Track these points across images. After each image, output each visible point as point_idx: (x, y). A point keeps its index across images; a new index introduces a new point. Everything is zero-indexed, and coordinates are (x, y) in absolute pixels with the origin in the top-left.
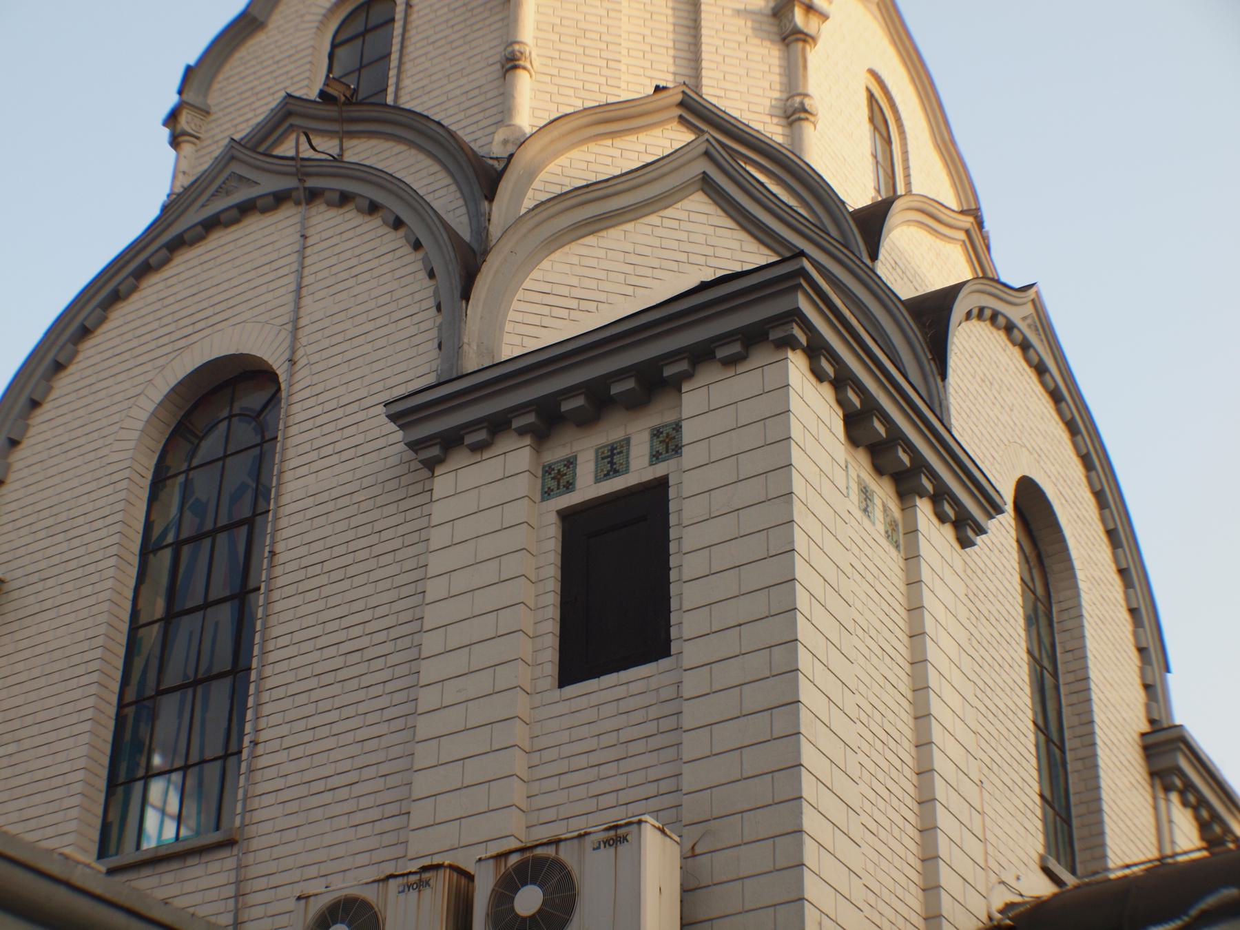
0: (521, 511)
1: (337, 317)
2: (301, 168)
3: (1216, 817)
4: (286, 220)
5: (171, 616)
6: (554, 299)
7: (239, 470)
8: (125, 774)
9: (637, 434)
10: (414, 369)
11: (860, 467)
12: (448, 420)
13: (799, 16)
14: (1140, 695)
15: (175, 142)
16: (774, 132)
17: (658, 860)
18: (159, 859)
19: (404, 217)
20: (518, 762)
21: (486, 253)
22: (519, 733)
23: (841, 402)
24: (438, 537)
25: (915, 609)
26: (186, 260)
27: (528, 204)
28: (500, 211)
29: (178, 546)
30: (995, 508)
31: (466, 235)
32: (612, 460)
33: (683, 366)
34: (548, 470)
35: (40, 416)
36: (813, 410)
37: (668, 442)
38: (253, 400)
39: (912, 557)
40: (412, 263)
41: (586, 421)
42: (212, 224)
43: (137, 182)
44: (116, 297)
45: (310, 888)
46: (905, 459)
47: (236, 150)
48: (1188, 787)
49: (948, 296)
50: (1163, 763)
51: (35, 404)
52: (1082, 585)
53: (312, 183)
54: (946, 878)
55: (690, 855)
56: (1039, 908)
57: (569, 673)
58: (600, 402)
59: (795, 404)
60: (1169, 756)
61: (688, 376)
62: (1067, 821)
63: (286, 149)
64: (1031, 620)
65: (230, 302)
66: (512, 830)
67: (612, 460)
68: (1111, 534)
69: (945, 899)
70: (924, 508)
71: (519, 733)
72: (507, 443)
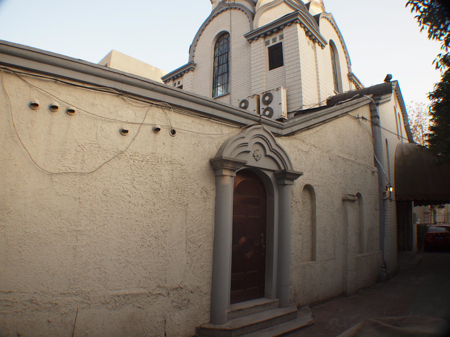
0: (263, 48)
1: (236, 24)
2: (229, 5)
3: (358, 85)
4: (228, 12)
5: (218, 66)
6: (265, 19)
7: (225, 46)
8: (215, 87)
9: (277, 36)
10: (247, 30)
11: (308, 39)
12: (252, 37)
14: (347, 69)
15: (212, 3)
17: (283, 92)
18: (220, 97)
19: (244, 10)
20: (265, 81)
21: (255, 14)
22: (264, 77)
23: (305, 30)
24: (252, 52)
26: (215, 19)
27: (260, 7)
28: (257, 8)
29: (218, 57)
30: (326, 44)
31: (252, 11)
32: (274, 40)
34: (266, 42)
35: (198, 42)
36: (301, 32)
37: (282, 37)
38: (226, 36)
39: (315, 51)
40: (245, 16)
41: (270, 35)
42: (218, 14)
43: (208, 9)
44: (207, 25)
45: (239, 99)
47: (220, 4)
48: (354, 81)
49: (319, 15)
50: (350, 78)
51: (198, 40)
52: (339, 54)
53: (231, 7)
54: (321, 93)
55: (287, 91)
56: (334, 97)
57: (270, 70)
58: (272, 32)
60: (351, 77)
61: (284, 28)
62: (337, 86)
63: (227, 2)
64: (332, 59)
65: (221, 24)
66: (265, 89)
67: (274, 40)
68: (343, 47)
69: (320, 88)
70: (317, 44)
71: (264, 77)
72: (260, 39)
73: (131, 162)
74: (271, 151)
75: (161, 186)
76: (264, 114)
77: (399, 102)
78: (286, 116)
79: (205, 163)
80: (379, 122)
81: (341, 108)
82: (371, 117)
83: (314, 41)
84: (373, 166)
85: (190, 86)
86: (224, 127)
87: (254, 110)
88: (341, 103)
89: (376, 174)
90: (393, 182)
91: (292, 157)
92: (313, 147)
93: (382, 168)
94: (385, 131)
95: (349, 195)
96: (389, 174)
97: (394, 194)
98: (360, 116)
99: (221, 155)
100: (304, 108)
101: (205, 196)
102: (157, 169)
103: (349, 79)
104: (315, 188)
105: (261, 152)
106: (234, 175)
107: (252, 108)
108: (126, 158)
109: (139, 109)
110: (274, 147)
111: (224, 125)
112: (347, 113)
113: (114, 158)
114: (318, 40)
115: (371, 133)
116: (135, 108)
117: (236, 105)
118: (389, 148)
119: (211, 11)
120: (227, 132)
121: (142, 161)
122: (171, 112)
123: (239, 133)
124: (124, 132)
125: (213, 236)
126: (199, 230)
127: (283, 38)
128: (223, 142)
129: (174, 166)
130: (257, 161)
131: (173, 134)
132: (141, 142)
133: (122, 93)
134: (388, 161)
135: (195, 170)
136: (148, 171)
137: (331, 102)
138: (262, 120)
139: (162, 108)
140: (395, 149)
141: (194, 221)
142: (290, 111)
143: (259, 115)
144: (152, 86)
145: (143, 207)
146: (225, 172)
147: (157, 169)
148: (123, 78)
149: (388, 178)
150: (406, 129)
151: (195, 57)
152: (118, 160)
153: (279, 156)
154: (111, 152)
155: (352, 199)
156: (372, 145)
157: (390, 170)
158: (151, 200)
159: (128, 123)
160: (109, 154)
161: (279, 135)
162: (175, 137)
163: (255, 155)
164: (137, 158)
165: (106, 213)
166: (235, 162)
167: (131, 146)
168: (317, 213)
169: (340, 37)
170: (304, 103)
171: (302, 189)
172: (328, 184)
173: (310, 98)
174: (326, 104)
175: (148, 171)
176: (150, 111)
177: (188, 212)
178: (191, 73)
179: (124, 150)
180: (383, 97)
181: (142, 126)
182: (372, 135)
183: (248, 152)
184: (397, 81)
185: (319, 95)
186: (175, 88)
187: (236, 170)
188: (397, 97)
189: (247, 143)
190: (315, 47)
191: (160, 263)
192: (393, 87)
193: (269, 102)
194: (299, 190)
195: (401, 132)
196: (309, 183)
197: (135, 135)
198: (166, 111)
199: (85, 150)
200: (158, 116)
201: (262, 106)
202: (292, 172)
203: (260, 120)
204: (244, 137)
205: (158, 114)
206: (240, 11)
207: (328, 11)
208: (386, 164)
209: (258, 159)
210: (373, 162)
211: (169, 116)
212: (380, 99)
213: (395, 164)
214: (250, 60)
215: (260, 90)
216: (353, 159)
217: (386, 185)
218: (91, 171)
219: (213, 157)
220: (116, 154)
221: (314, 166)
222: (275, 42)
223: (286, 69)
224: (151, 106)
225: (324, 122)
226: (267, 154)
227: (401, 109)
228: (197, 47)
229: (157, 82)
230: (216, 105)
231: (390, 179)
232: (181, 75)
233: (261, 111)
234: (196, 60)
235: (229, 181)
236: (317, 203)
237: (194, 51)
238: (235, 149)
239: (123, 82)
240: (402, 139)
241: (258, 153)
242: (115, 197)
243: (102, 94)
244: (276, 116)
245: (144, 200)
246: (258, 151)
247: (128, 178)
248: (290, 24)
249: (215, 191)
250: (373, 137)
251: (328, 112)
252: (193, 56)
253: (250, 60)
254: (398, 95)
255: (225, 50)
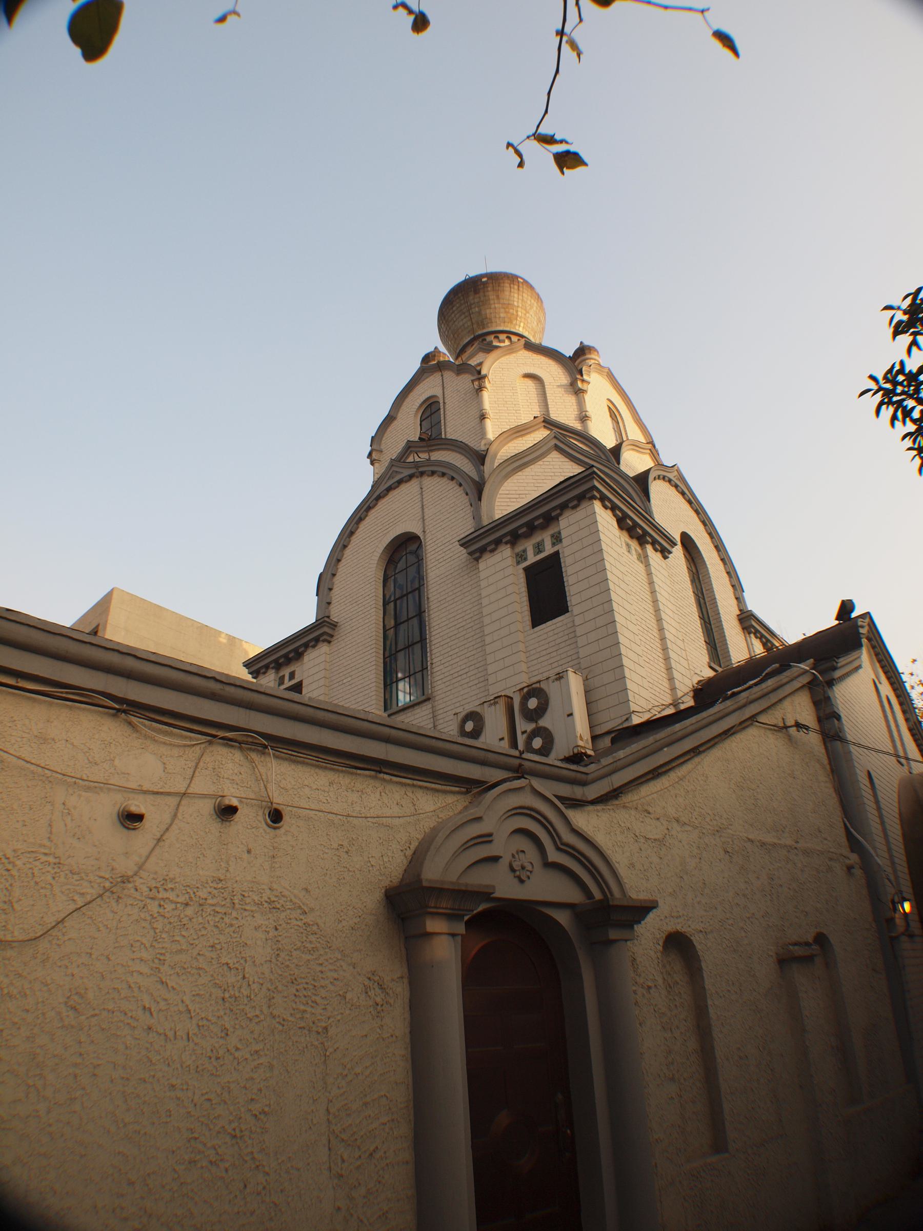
0: (510, 570)
1: (437, 514)
2: (416, 465)
3: (768, 640)
4: (414, 483)
5: (397, 626)
6: (510, 496)
7: (412, 571)
8: (389, 683)
9: (545, 537)
10: (466, 527)
11: (624, 537)
12: (481, 543)
13: (580, 384)
15: (372, 463)
16: (577, 426)
17: (575, 683)
20: (522, 656)
21: (484, 484)
22: (521, 646)
23: (615, 515)
24: (483, 584)
25: (651, 583)
26: (382, 503)
27: (496, 464)
28: (487, 468)
29: (395, 601)
30: (674, 544)
32: (539, 548)
33: (558, 511)
34: (517, 555)
36: (605, 520)
37: (557, 539)
38: (413, 547)
39: (647, 565)
40: (459, 492)
41: (528, 535)
42: (389, 489)
46: (640, 532)
47: (393, 463)
50: (746, 624)
53: (421, 469)
55: (586, 680)
56: (710, 681)
57: (535, 624)
58: (531, 529)
59: (599, 518)
61: (560, 514)
63: (410, 459)
64: (693, 581)
65: (400, 514)
66: (524, 680)
67: (539, 548)
68: (716, 547)
70: (649, 548)
73: (153, 907)
74: (558, 849)
75: (244, 978)
76: (529, 748)
77: (882, 667)
78: (590, 745)
79: (373, 900)
80: (841, 729)
81: (736, 706)
82: (819, 720)
83: (642, 539)
84: (846, 851)
85: (322, 682)
86: (420, 794)
87: (502, 739)
88: (734, 694)
89: (858, 872)
90: (906, 886)
91: (620, 860)
92: (675, 825)
93: (872, 851)
94: (860, 750)
95: (795, 944)
96: (893, 863)
97: (917, 918)
98: (791, 722)
99: (419, 875)
100: (636, 720)
101: (378, 1000)
102: (231, 925)
103: (743, 629)
104: (697, 940)
105: (531, 855)
106: (461, 928)
107: (494, 733)
108: (137, 895)
109: (176, 752)
110: (568, 837)
111: (420, 787)
112: (753, 719)
113: (101, 896)
114: (651, 536)
115: (826, 762)
116: (163, 750)
117: (449, 728)
118: (879, 794)
119: (371, 483)
120: (430, 807)
121: (187, 904)
122: (268, 759)
123: (466, 808)
124: (131, 819)
125: (412, 1117)
126: (366, 1104)
127: (561, 541)
128: (420, 837)
129: (283, 915)
130: (522, 881)
131: (274, 821)
132: (185, 847)
133: (125, 708)
134: (884, 830)
135: (344, 923)
136: (204, 932)
137: (706, 694)
138: (526, 764)
139: (241, 748)
140: (896, 795)
141: (350, 1078)
142: (599, 731)
143: (516, 753)
144: (212, 685)
145: (191, 1045)
146: (433, 925)
147: (231, 925)
148: (130, 663)
149: (892, 877)
150: (913, 735)
151: (332, 606)
152: (114, 904)
153: (584, 861)
154: (92, 877)
155: (803, 955)
156: (834, 795)
157: (895, 854)
158: (214, 1020)
159: (145, 792)
160: (85, 884)
161: (577, 804)
162: (282, 831)
163: (516, 865)
164: (172, 895)
165: (76, 1065)
166: (459, 891)
167: (153, 859)
168: (711, 1011)
169: (706, 522)
170: (633, 707)
171: (660, 948)
172: (730, 922)
173: (649, 689)
174: (691, 703)
175: (204, 932)
176: (207, 758)
177: (331, 1050)
178: (323, 648)
179: (130, 873)
180: (842, 661)
181: (183, 802)
182: (828, 767)
183: (495, 859)
184: (868, 613)
185: (671, 679)
186: (280, 691)
187: (463, 915)
188: (877, 655)
189: (490, 835)
190: (646, 556)
191: (252, 1213)
192: (861, 631)
193: (542, 710)
194: (652, 953)
195: (903, 744)
196: (679, 928)
197: (164, 827)
198: (254, 755)
199: (14, 872)
200: (229, 772)
201: (522, 726)
202: (625, 903)
203: (520, 765)
204: (479, 819)
205: (230, 765)
206: (445, 480)
207: (667, 461)
208: (879, 840)
209: (524, 877)
210: (844, 840)
211: (263, 770)
212: (835, 669)
213: (904, 835)
214: (477, 603)
215: (511, 678)
216: (790, 842)
217: (890, 897)
218: (32, 935)
219: (396, 881)
220: (108, 885)
221: (685, 877)
222: (540, 552)
223: (578, 621)
224: (210, 743)
225: (696, 751)
226: (550, 860)
227: (892, 684)
228: (336, 579)
229: (227, 675)
230: (393, 732)
231: (897, 877)
232: (298, 655)
233: (521, 740)
234: (335, 614)
235: (445, 949)
236: (708, 983)
237: (331, 589)
238: (456, 855)
239: (129, 675)
240: (909, 764)
241: (524, 859)
242: (105, 1013)
243: (70, 708)
244: (561, 749)
245: (194, 1021)
246: (521, 855)
247: (145, 955)
248: (575, 502)
249: (406, 981)
250: (832, 771)
251: (704, 722)
252: (329, 603)
253: (477, 603)
254: (878, 650)
255: (412, 582)
